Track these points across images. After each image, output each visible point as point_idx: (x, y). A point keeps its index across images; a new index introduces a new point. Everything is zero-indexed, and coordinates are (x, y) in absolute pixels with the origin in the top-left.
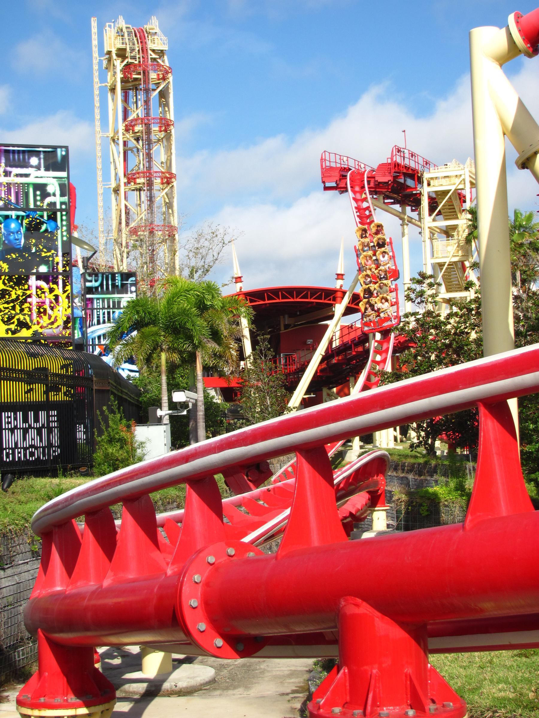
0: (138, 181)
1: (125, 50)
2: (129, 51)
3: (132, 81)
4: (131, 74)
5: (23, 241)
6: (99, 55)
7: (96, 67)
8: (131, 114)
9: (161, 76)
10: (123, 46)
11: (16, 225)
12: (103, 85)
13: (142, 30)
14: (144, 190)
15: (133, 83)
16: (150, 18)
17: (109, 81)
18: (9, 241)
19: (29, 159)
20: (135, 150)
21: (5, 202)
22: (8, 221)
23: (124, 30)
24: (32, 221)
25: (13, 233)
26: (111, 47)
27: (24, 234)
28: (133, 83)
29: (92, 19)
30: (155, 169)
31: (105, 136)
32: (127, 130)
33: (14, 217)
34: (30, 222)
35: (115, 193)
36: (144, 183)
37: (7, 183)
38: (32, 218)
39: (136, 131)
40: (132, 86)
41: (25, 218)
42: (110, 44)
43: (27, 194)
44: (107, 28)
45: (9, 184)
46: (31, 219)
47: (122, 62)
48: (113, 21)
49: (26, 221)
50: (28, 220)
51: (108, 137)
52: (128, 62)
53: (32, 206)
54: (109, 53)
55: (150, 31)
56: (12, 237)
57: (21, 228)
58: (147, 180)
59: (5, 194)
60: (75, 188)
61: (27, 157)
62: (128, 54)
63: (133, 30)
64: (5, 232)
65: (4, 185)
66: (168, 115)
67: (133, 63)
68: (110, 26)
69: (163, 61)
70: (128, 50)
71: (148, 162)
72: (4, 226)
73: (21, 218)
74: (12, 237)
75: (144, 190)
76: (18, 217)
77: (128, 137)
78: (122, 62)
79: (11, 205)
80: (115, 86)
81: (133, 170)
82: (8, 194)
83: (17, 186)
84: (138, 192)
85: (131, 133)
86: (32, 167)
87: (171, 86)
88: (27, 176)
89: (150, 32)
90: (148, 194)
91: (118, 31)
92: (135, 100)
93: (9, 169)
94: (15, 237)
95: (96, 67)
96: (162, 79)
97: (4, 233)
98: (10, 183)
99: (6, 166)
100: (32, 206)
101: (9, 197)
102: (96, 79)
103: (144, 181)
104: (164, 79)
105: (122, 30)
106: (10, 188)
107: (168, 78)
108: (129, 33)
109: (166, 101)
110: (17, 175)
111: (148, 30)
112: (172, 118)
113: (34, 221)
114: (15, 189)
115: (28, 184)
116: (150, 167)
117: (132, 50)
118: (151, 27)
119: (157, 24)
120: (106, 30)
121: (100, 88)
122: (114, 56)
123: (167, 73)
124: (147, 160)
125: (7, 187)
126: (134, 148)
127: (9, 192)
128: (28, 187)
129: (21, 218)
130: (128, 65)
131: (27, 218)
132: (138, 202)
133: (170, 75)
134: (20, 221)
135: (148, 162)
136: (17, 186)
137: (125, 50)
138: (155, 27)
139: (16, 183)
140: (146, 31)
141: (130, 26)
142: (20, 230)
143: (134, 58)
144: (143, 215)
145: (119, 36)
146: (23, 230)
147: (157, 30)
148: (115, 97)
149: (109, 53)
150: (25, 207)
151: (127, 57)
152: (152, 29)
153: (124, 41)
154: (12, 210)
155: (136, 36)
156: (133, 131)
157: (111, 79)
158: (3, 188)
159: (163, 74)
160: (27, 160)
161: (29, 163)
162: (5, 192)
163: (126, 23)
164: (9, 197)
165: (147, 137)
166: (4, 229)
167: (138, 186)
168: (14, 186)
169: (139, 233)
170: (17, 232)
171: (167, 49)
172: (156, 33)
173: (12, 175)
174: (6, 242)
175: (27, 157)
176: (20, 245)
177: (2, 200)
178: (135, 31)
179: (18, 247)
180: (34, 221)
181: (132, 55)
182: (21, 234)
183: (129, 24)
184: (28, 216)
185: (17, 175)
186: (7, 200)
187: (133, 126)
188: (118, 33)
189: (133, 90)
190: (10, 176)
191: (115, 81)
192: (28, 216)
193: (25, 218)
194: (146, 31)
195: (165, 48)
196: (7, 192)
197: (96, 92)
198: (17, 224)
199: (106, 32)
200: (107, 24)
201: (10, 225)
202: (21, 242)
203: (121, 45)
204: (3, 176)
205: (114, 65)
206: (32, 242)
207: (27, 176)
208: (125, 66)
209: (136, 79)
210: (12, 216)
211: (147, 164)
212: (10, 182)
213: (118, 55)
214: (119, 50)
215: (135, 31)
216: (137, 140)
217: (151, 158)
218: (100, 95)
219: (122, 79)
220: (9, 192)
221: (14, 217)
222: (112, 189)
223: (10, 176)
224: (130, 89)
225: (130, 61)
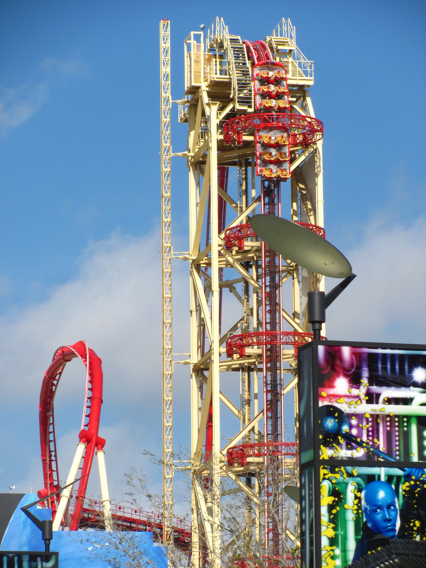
0: (248, 351)
1: (228, 85)
2: (237, 88)
3: (240, 148)
4: (239, 133)
5: (398, 524)
6: (172, 94)
7: (166, 119)
8: (236, 218)
9: (300, 138)
10: (224, 78)
11: (386, 493)
12: (180, 154)
13: (263, 46)
14: (261, 370)
15: (241, 152)
16: (279, 21)
17: (191, 146)
18: (375, 523)
19: (411, 370)
20: (240, 287)
21: (369, 451)
22: (372, 485)
23: (227, 44)
24: (415, 486)
25: (380, 507)
26: (197, 78)
27: (401, 511)
28: (241, 152)
29: (162, 23)
30: (284, 327)
31: (182, 257)
32: (228, 247)
33: (383, 479)
34: (412, 488)
35: (197, 376)
36: (260, 356)
37: (372, 415)
38: (415, 481)
39: (246, 248)
40: (239, 156)
41: (403, 480)
42: (197, 73)
43: (406, 436)
44: (193, 42)
45: (375, 417)
46: (412, 483)
47: (221, 109)
48: (202, 26)
49: (404, 487)
50: (407, 484)
51: (186, 259)
52: (233, 109)
53: (415, 458)
54: (194, 90)
55: (280, 47)
56: (379, 517)
57: (396, 500)
58: (267, 350)
59: (368, 436)
60: (100, 361)
61: (406, 367)
62: (234, 93)
63: (244, 46)
64: (368, 507)
65: (367, 419)
66: (312, 218)
67: (245, 110)
68: (197, 38)
69: (304, 107)
70: (235, 84)
71: (270, 312)
72: (366, 496)
73: (395, 480)
74: (379, 517)
75: (261, 370)
76: (390, 478)
77: (231, 260)
78: (221, 109)
79: (379, 456)
80: (205, 156)
81: (235, 328)
82: (373, 436)
83: (390, 421)
84: (246, 374)
85: (234, 253)
86: (416, 385)
87: (320, 162)
88: (407, 401)
89: (278, 50)
90: (269, 378)
91: (212, 46)
92: (244, 188)
93: (375, 389)
94: (384, 516)
95: (166, 119)
96: (301, 144)
97: (366, 509)
98: (378, 416)
99: (371, 382)
100: (415, 458)
101: (376, 440)
102: (166, 144)
103: (259, 351)
104: (306, 144)
105: (221, 46)
106: (378, 424)
107: (315, 143)
108: (238, 52)
109: (307, 189)
110: (390, 401)
111: (274, 46)
112: (321, 224)
113: (418, 486)
114: (385, 426)
115: (409, 417)
116: (273, 323)
117: (243, 86)
118: (280, 38)
119: (294, 34)
120: (189, 45)
121: (173, 159)
122: (206, 99)
123: (313, 131)
124: (268, 308)
125: (372, 422)
126: (237, 281)
127: (374, 432)
128: (408, 422)
129: (395, 480)
130: (233, 114)
131: (405, 481)
132: (246, 397)
133: (318, 136)
134: (393, 486)
135: (270, 312)
136: (390, 421)
137: (228, 85)
138: (288, 40)
139: (388, 416)
140: (271, 48)
141: (239, 37)
142: (393, 504)
143: (246, 101)
144: (255, 423)
145: (215, 56)
146: (398, 503)
147: (292, 46)
148: (204, 180)
149: (194, 90)
150: (402, 460)
151: (233, 100)
152: (283, 43)
153: (226, 67)
154: (379, 465)
155: (250, 58)
156: (241, 248)
157: (196, 143)
158: (364, 423)
159: (304, 134)
160: (407, 374)
161: (411, 378)
162: (368, 431)
163: (231, 32)
164: (376, 440)
165: (269, 262)
166: (366, 501)
167: (245, 362)
168: (385, 421)
169: (249, 459)
170: (389, 507)
171: (311, 83)
172: (290, 51)
173: (381, 400)
174: (369, 525)
175: (406, 367)
176: (394, 530)
177: (363, 447)
178: (248, 48)
179: (390, 534)
180: (418, 486)
181: (242, 95)
182: (395, 510)
183: (237, 34)
184: (408, 478)
185: (390, 401)
186: (373, 446)
187: (240, 239)
188: (212, 49)
189: (241, 166)
190: (377, 403)
191: (207, 147)
192: (408, 478)
193: (403, 480)
194: (271, 48)
195: (309, 81)
196: (372, 431)
197: (166, 169)
198: (389, 491)
199: (189, 49)
200: (192, 33)
201: (376, 493)
202: (395, 525)
203: (218, 76)
204: (364, 402)
205: (203, 114)
206: (415, 525)
207: (407, 401)
208: (228, 116)
209: (248, 144)
210: (379, 476)
211: (268, 316)
212: (378, 413)
213: (212, 96)
214: (214, 84)
215: (248, 48)
216: (247, 266)
217: (276, 304)
218: (173, 174)
219: (220, 143)
220: (374, 432)
221: (383, 479)
222: (192, 366)
223: (377, 403)
224: (234, 164)
225: (238, 107)
